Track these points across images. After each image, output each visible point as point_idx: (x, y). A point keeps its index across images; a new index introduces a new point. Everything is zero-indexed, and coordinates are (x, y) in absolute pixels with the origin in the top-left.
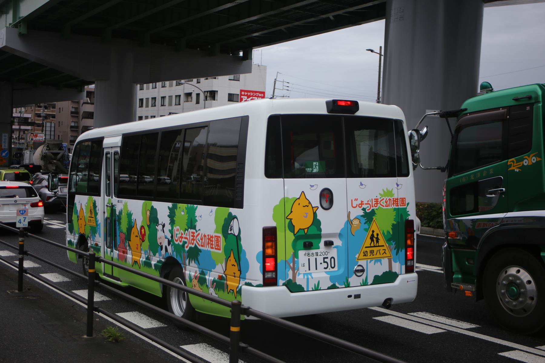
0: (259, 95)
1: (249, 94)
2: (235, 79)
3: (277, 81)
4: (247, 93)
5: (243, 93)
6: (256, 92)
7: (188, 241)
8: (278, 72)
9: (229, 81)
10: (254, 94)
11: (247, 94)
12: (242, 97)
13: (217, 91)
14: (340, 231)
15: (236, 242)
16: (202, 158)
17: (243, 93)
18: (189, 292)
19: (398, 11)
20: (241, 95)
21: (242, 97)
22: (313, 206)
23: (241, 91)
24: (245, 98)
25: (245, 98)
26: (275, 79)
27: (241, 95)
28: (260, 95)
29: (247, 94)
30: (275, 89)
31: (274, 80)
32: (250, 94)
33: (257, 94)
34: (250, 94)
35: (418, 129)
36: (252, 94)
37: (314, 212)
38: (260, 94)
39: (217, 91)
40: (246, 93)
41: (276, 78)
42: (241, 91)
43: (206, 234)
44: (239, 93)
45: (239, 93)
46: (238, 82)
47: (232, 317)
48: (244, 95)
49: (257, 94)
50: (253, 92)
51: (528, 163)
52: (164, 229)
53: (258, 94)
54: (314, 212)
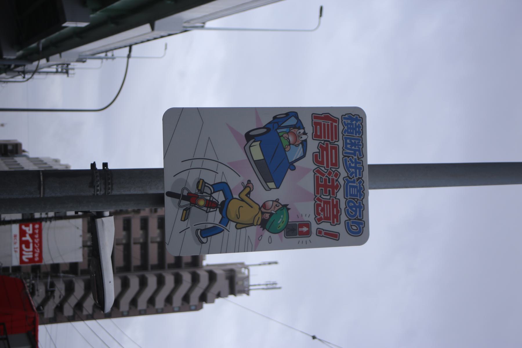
0: (37, 253)
1: (37, 236)
6: (41, 248)
7: (323, 193)
8: (168, 245)
9: (180, 233)
10: (37, 245)
14: (227, 296)
19: (337, 180)
22: (134, 48)
24: (29, 230)
25: (29, 230)
28: (36, 255)
30: (245, 228)
32: (36, 238)
34: (36, 238)
35: (181, 255)
36: (37, 241)
37: (189, 210)
40: (37, 231)
48: (34, 229)
50: (40, 242)
51: (297, 131)
54: (189, 210)
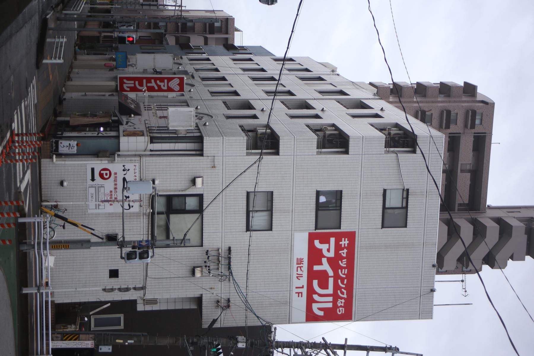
1: (343, 263)
2: (386, 211)
3: (345, 353)
4: (345, 255)
5: (344, 242)
10: (343, 283)
11: (342, 258)
12: (332, 240)
13: (347, 152)
15: (479, 277)
16: (152, 140)
17: (344, 242)
18: (3, 154)
20: (339, 237)
21: (332, 240)
23: (351, 236)
24: (328, 250)
26: (398, 349)
27: (339, 237)
29: (342, 258)
31: (393, 346)
32: (342, 268)
33: (345, 291)
34: (342, 268)
36: (342, 273)
38: (343, 301)
39: (347, 152)
40: (344, 253)
41: (400, 350)
42: (351, 236)
43: (114, 180)
44: (345, 228)
45: (345, 228)
46: (244, 228)
47: (312, 295)
48: (338, 247)
49: (343, 293)
50: (350, 276)
52: (202, 37)
53: (345, 296)
